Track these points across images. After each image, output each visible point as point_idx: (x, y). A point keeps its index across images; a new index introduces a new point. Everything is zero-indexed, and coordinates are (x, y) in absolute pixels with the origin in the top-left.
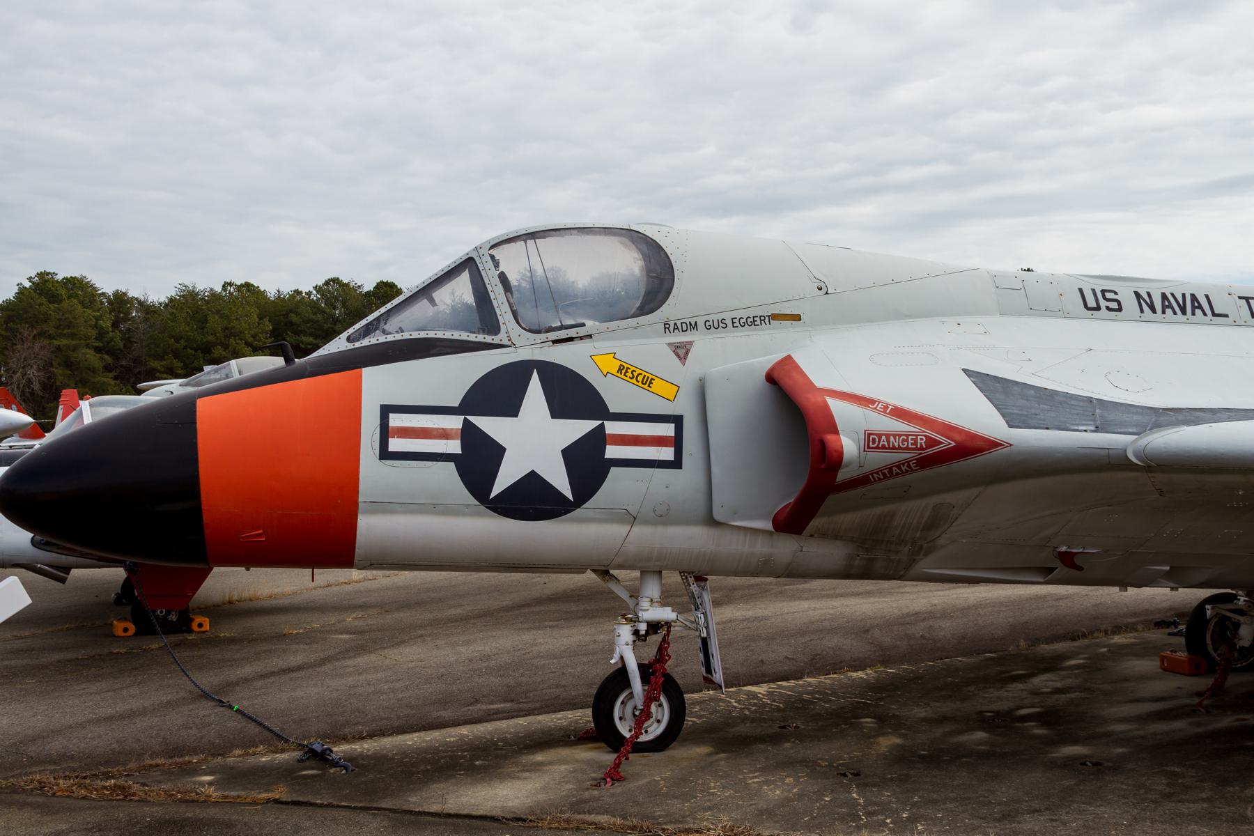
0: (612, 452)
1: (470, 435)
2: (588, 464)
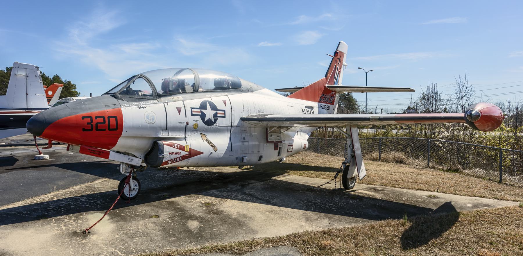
0: (218, 115)
1: (201, 112)
2: (216, 116)
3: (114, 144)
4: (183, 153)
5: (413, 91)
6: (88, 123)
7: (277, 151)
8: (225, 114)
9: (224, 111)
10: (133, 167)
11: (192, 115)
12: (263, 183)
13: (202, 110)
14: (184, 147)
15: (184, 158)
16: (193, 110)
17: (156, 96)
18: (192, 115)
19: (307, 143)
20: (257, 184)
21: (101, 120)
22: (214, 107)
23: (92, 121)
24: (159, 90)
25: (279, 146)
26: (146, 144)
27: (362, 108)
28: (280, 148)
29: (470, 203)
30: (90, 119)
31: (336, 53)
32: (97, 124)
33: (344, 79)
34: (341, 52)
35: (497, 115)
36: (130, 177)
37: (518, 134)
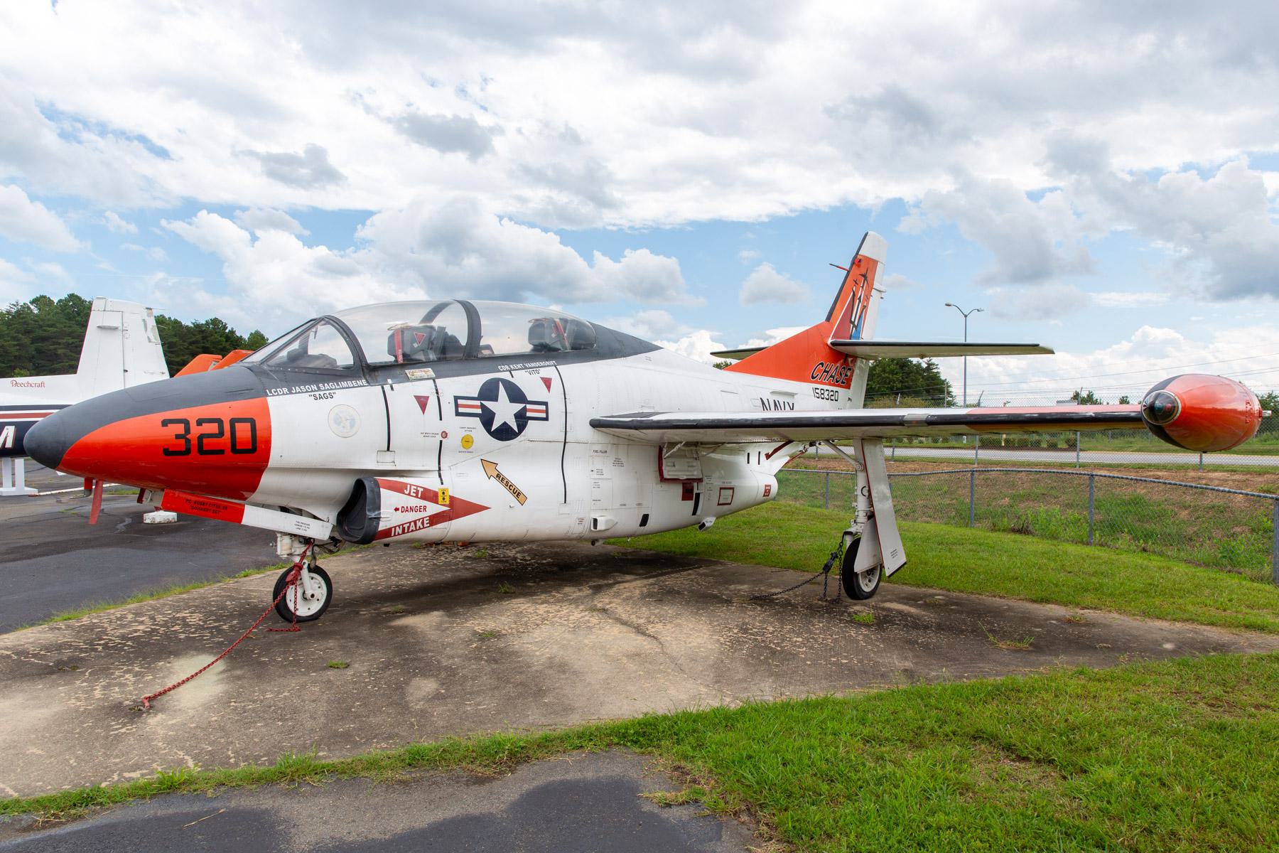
0: (529, 414)
1: (483, 407)
2: (522, 419)
3: (253, 487)
4: (433, 509)
5: (1052, 352)
6: (178, 437)
7: (691, 504)
8: (547, 411)
9: (546, 404)
10: (307, 541)
11: (458, 414)
12: (651, 581)
13: (485, 403)
14: (436, 494)
15: (435, 519)
16: (460, 402)
17: (364, 370)
18: (458, 414)
19: (774, 483)
20: (634, 583)
21: (212, 428)
22: (516, 395)
23: (188, 430)
24: (377, 352)
25: (695, 491)
26: (343, 486)
27: (959, 400)
28: (698, 495)
29: (1168, 641)
30: (248, 426)
31: (857, 262)
32: (201, 437)
33: (882, 325)
34: (869, 260)
35: (1241, 407)
36: (299, 567)
37: (104, 506)
